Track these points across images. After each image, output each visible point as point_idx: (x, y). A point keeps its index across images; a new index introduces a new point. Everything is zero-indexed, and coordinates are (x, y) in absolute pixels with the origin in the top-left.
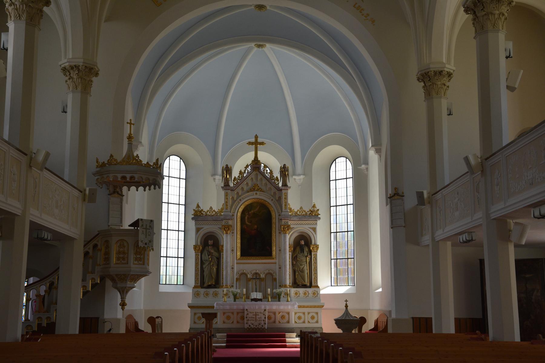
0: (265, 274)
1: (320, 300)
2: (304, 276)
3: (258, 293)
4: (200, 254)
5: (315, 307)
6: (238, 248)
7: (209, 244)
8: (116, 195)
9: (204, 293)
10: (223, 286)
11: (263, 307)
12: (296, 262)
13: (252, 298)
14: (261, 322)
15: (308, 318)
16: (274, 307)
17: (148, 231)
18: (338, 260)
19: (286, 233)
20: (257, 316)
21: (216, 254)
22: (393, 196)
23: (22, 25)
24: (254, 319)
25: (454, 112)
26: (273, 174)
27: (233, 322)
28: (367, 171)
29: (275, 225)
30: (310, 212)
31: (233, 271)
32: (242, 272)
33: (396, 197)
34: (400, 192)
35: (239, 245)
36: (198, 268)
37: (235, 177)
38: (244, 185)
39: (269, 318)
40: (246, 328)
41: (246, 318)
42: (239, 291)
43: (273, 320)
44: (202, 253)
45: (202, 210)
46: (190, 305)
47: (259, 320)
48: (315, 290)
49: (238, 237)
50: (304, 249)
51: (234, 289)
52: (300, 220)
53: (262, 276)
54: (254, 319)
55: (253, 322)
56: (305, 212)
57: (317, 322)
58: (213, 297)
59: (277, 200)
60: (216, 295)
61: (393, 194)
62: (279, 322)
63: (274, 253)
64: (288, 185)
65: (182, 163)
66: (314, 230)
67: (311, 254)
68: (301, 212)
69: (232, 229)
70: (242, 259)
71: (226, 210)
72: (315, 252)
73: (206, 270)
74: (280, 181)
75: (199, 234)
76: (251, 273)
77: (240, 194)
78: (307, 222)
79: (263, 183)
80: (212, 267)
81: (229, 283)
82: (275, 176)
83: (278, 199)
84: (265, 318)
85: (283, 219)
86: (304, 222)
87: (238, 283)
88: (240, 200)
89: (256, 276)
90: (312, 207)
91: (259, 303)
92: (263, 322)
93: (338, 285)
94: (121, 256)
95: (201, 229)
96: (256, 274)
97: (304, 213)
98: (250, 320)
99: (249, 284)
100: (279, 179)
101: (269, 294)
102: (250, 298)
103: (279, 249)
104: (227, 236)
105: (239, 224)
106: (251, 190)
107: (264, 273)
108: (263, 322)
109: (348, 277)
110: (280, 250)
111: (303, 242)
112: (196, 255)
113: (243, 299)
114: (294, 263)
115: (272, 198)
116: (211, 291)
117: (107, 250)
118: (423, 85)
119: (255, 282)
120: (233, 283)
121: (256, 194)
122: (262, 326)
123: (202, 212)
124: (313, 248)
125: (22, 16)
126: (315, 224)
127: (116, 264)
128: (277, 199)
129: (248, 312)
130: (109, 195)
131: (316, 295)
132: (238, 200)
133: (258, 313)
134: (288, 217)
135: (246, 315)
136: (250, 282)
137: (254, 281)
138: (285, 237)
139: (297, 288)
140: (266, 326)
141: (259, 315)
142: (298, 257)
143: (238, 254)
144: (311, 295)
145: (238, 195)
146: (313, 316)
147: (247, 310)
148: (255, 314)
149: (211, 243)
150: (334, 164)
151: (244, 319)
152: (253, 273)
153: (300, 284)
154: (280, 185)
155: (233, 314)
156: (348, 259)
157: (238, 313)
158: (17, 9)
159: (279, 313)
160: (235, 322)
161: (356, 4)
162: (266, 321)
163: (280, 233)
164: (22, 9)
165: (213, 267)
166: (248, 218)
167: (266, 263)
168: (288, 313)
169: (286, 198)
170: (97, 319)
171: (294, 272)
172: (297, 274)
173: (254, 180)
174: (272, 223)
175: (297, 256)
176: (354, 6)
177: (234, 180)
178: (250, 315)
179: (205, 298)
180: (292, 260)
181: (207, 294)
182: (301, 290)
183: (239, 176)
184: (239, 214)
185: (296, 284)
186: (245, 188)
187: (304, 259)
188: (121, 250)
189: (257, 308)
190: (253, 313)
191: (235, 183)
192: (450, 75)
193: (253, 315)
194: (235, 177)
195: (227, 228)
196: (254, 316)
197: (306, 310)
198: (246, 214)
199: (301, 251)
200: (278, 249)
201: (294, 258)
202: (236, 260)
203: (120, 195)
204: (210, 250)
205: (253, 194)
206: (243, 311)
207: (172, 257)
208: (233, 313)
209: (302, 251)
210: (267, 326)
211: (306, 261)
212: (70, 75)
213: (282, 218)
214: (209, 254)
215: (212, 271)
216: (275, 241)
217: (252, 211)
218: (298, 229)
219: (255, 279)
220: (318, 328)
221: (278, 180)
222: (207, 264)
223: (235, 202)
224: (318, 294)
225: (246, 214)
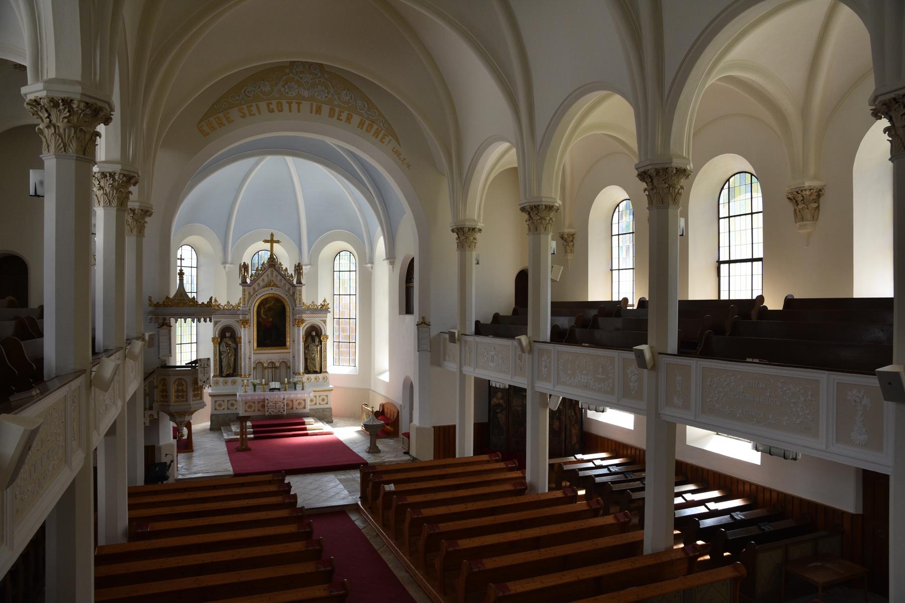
8: (165, 327)
11: (282, 397)
15: (319, 400)
16: (292, 396)
17: (206, 369)
21: (233, 345)
22: (420, 324)
23: (113, 211)
25: (480, 262)
27: (254, 411)
28: (372, 269)
29: (290, 318)
32: (258, 361)
33: (423, 325)
34: (427, 321)
35: (255, 337)
36: (217, 359)
38: (260, 281)
39: (288, 405)
44: (220, 344)
45: (220, 304)
46: (211, 394)
53: (277, 364)
57: (327, 403)
59: (291, 296)
60: (234, 383)
61: (420, 323)
62: (297, 408)
63: (288, 344)
64: (302, 282)
66: (325, 322)
67: (321, 344)
71: (244, 306)
73: (224, 360)
77: (256, 290)
78: (318, 315)
79: (278, 279)
81: (247, 373)
82: (290, 274)
84: (284, 406)
88: (257, 295)
89: (273, 366)
91: (276, 392)
92: (282, 410)
94: (180, 394)
100: (294, 276)
104: (245, 330)
105: (255, 318)
108: (282, 410)
110: (294, 341)
112: (214, 346)
114: (306, 352)
115: (287, 293)
116: (230, 379)
117: (164, 388)
118: (457, 236)
121: (272, 289)
125: (112, 202)
127: (176, 402)
128: (291, 294)
130: (159, 328)
132: (255, 295)
134: (303, 312)
136: (266, 371)
138: (299, 330)
139: (308, 374)
145: (255, 291)
147: (267, 399)
150: (338, 256)
154: (295, 282)
156: (350, 342)
157: (259, 402)
158: (106, 194)
159: (296, 400)
160: (256, 410)
161: (394, 148)
163: (294, 325)
164: (113, 195)
166: (264, 312)
168: (305, 400)
169: (300, 295)
170: (153, 447)
171: (306, 360)
172: (309, 361)
173: (270, 276)
176: (393, 150)
177: (251, 277)
178: (271, 404)
181: (226, 383)
182: (313, 376)
185: (307, 371)
186: (262, 284)
188: (180, 388)
189: (277, 397)
192: (480, 230)
195: (245, 322)
197: (317, 394)
200: (292, 340)
201: (306, 348)
202: (253, 350)
203: (168, 326)
204: (228, 342)
206: (264, 400)
208: (254, 403)
209: (314, 341)
211: (317, 350)
212: (48, 117)
217: (268, 305)
218: (309, 322)
221: (293, 277)
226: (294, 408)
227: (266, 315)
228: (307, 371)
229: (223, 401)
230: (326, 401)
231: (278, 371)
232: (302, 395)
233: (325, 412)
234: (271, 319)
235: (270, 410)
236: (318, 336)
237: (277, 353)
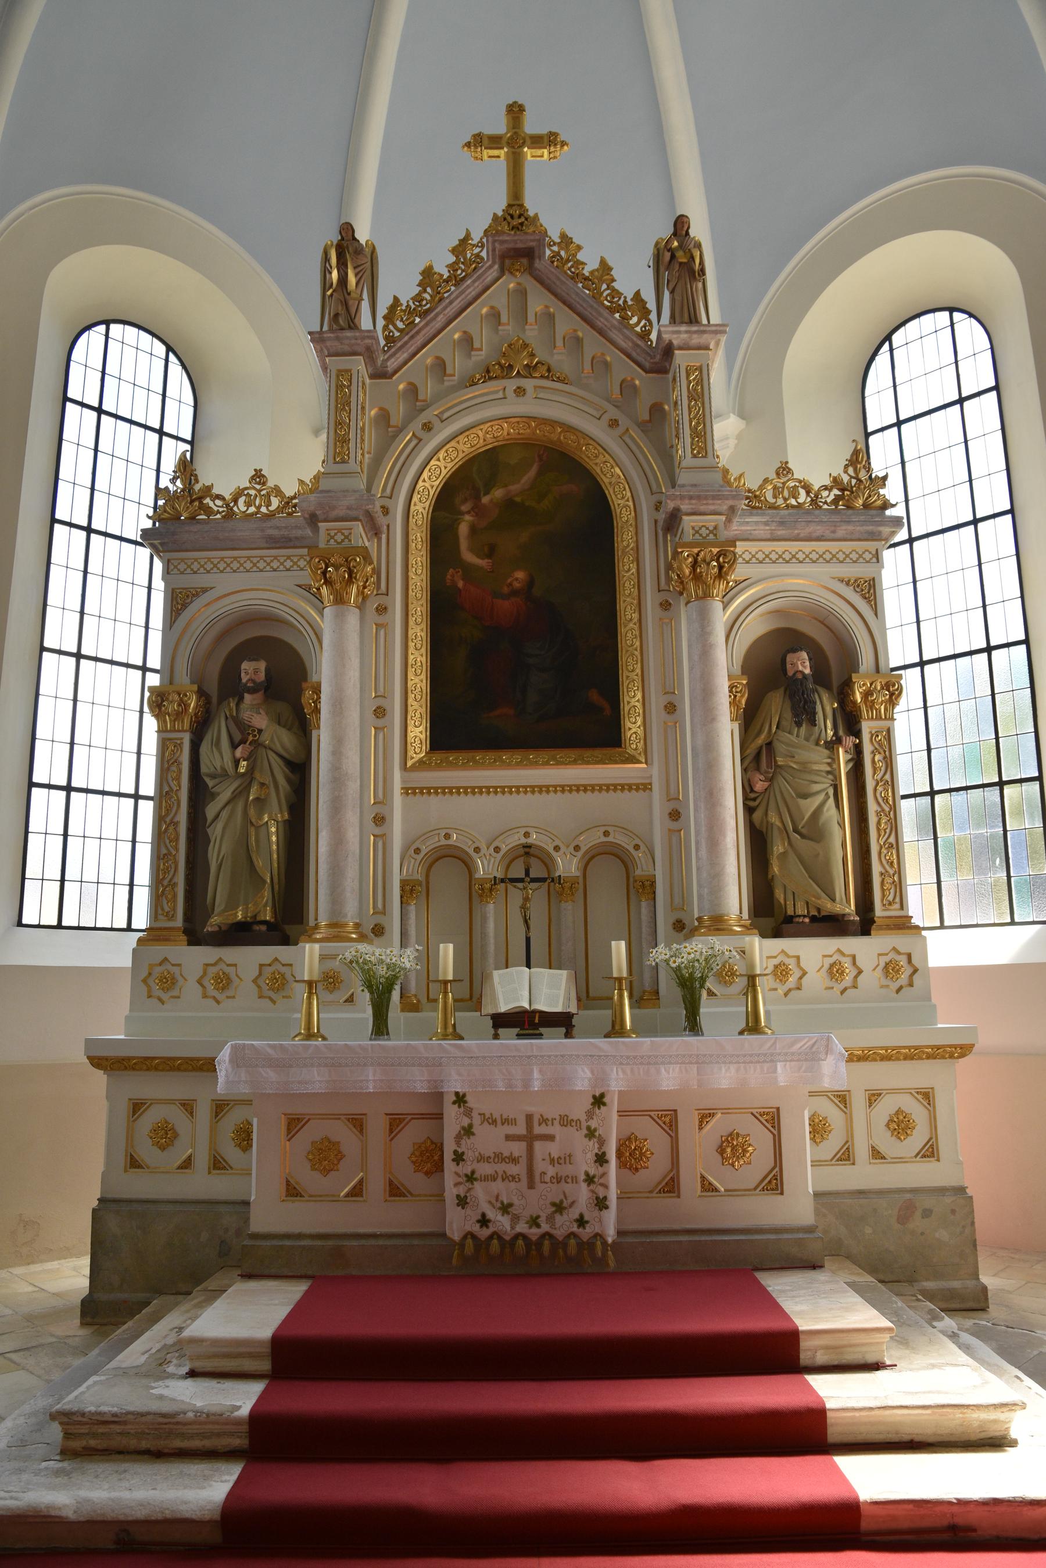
0: (580, 854)
1: (935, 1006)
2: (827, 866)
3: (543, 974)
4: (186, 738)
5: (913, 1054)
6: (410, 701)
7: (244, 678)
9: (205, 973)
10: (317, 927)
11: (583, 1079)
12: (771, 780)
13: (503, 1008)
14: (568, 1188)
18: (937, 798)
19: (707, 595)
20: (538, 1145)
21: (283, 739)
24: (513, 1169)
26: (613, 280)
27: (357, 1192)
30: (836, 492)
31: (383, 839)
35: (420, 682)
37: (396, 300)
40: (457, 1237)
41: (459, 1158)
42: (407, 959)
43: (656, 1168)
44: (199, 730)
47: (558, 1179)
48: (839, 951)
49: (411, 661)
50: (815, 703)
51: (371, 951)
52: (781, 532)
53: (567, 865)
54: (513, 1169)
55: (506, 1191)
56: (808, 489)
57: (930, 1152)
58: (205, 996)
59: (643, 426)
62: (708, 1187)
63: (632, 727)
65: (175, 367)
67: (855, 731)
68: (786, 493)
69: (378, 587)
70: (439, 767)
72: (879, 718)
74: (653, 317)
75: (188, 625)
76: (497, 850)
78: (821, 546)
80: (252, 812)
83: (647, 418)
84: (601, 1159)
85: (685, 507)
86: (808, 547)
87: (412, 909)
88: (427, 427)
90: (846, 467)
91: (552, 1043)
92: (583, 1194)
93: (946, 924)
95: (197, 595)
96: (527, 850)
97: (803, 497)
98: (486, 1178)
99: (484, 920)
100: (652, 305)
101: (620, 980)
102: (488, 1009)
103: (664, 700)
104: (340, 618)
105: (420, 559)
106: (488, 371)
107: (577, 848)
108: (583, 1194)
109: (1009, 877)
110: (671, 708)
111: (807, 663)
113: (436, 1010)
114: (760, 786)
115: (613, 413)
119: (520, 902)
120: (384, 913)
121: (520, 391)
122: (581, 1222)
123: (207, 501)
124: (867, 694)
126: (867, 556)
129: (468, 1112)
131: (904, 978)
132: (416, 425)
133: (543, 1121)
135: (458, 1138)
136: (491, 907)
137: (516, 895)
138: (704, 620)
139: (777, 934)
140: (609, 1225)
141: (551, 1138)
142: (780, 747)
143: (410, 735)
144: (872, 978)
146: (899, 1112)
147: (460, 1099)
148: (521, 1129)
149: (256, 671)
150: (883, 358)
151: (439, 1167)
152: (504, 849)
153: (801, 910)
155: (361, 1131)
156: (1001, 784)
157: (396, 1123)
159: (705, 1117)
160: (376, 1187)
162: (606, 1186)
163: (666, 606)
165: (260, 818)
166: (473, 530)
167: (585, 788)
168: (772, 1120)
172: (778, 848)
174: (618, 553)
175: (769, 744)
179: (211, 1002)
180: (745, 770)
183: (418, 298)
184: (422, 507)
186: (458, 365)
187: (818, 757)
189: (536, 1086)
190: (506, 1121)
191: (397, 334)
193: (508, 1138)
194: (396, 300)
196: (518, 1149)
198: (464, 508)
199: (796, 715)
200: (657, 702)
202: (404, 767)
204: (246, 715)
205: (500, 395)
207: (103, 793)
208: (358, 1123)
210: (619, 1219)
211: (834, 774)
213: (682, 498)
214: (238, 737)
215: (257, 841)
216: (637, 653)
217: (498, 493)
219: (521, 880)
220: (942, 1191)
221: (645, 313)
222: (225, 795)
223: (395, 437)
224: (145, 981)
225: (464, 508)
226: (689, 1183)
227: (490, 552)
228: (768, 922)
229: (188, 1107)
230: (918, 1139)
231: (570, 911)
232: (755, 1076)
233: (917, 1223)
234: (520, 575)
235: (479, 1191)
236: (828, 687)
237: (563, 788)
